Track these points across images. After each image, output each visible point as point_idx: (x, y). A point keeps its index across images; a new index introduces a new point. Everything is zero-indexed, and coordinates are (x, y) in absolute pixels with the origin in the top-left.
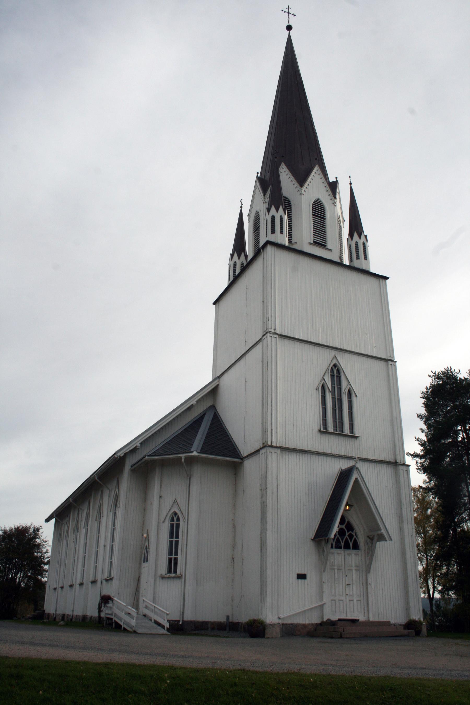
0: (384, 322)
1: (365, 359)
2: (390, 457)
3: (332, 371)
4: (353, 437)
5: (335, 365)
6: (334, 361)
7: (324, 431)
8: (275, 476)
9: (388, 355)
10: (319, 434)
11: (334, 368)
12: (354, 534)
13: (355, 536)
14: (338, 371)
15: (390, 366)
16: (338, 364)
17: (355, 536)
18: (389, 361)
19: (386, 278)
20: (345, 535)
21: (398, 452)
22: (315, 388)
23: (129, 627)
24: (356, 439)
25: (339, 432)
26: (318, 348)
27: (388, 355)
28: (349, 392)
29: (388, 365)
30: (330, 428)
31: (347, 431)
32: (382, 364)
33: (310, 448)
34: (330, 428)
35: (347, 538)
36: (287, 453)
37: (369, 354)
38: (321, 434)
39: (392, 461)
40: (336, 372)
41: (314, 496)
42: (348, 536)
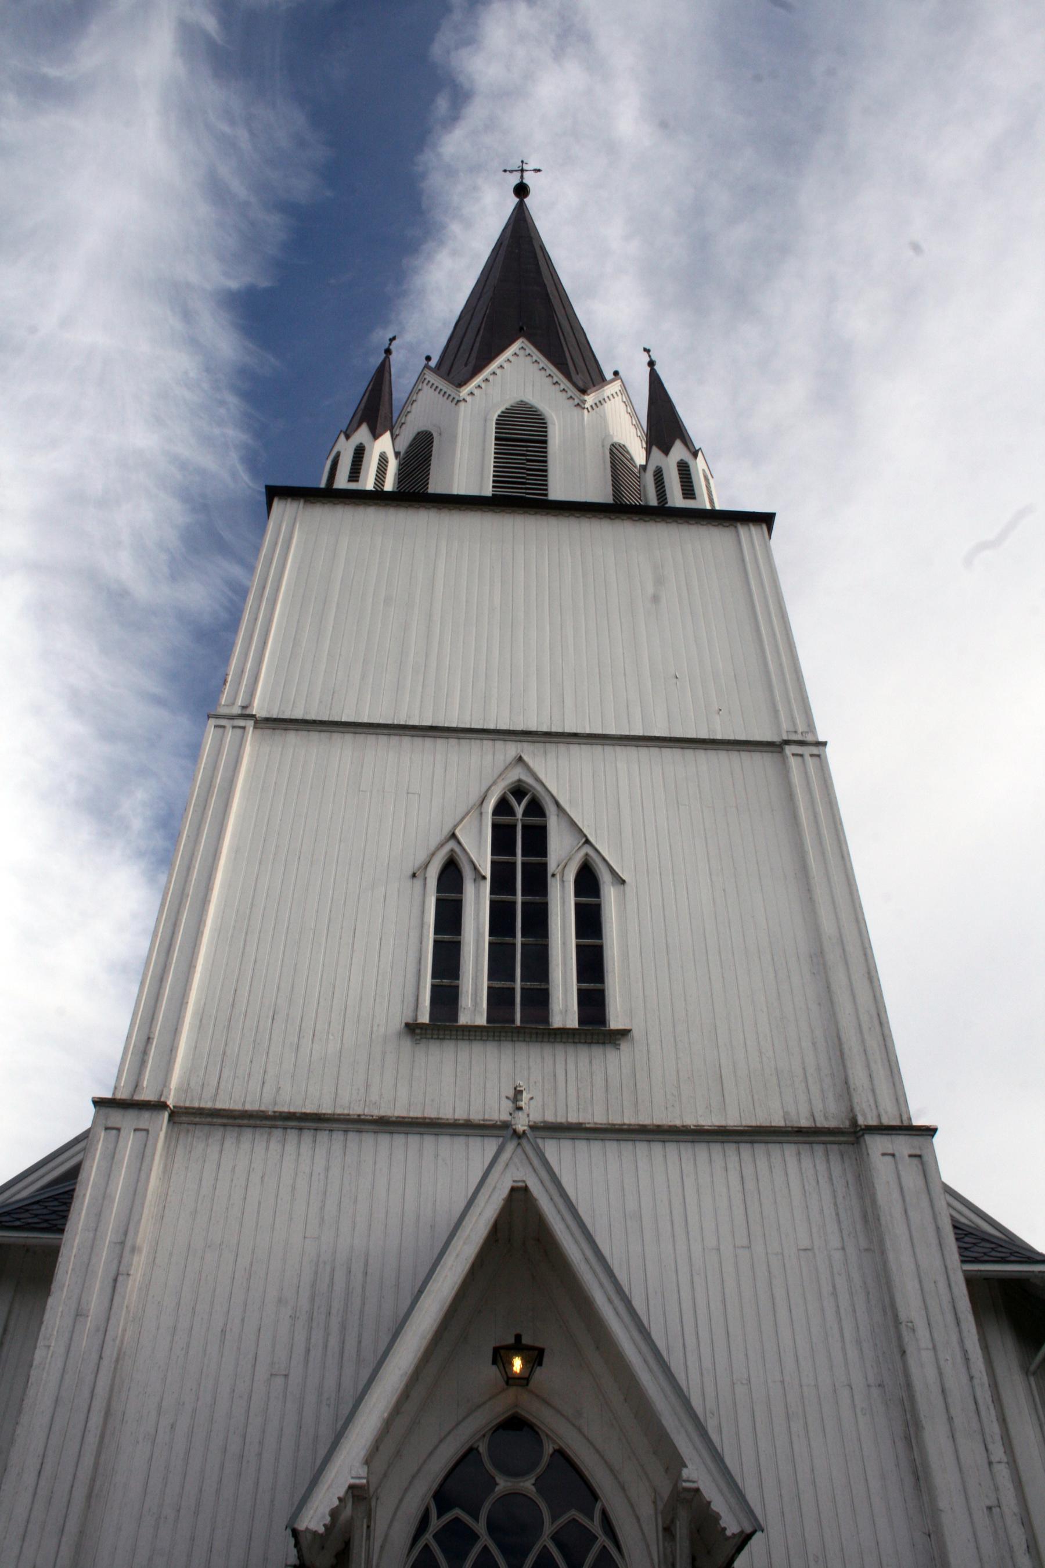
0: (757, 630)
1: (670, 755)
2: (818, 1106)
3: (503, 807)
4: (595, 1026)
5: (519, 791)
6: (517, 774)
7: (440, 1022)
8: (110, 1233)
9: (785, 726)
10: (407, 1043)
11: (513, 800)
12: (595, 1526)
13: (435, 1524)
14: (536, 808)
15: (793, 762)
16: (530, 781)
17: (603, 1539)
18: (789, 748)
19: (766, 520)
20: (492, 1528)
21: (858, 1076)
22: (410, 873)
23: (1030, 1385)
24: (617, 1046)
25: (519, 1014)
26: (439, 741)
27: (785, 726)
28: (587, 881)
29: (784, 761)
30: (474, 1005)
31: (564, 1008)
32: (760, 763)
33: (349, 1101)
34: (474, 1005)
35: (545, 1552)
36: (218, 1133)
37: (691, 734)
38: (417, 1042)
39: (832, 1124)
40: (522, 823)
41: (343, 1327)
42: (555, 1538)
